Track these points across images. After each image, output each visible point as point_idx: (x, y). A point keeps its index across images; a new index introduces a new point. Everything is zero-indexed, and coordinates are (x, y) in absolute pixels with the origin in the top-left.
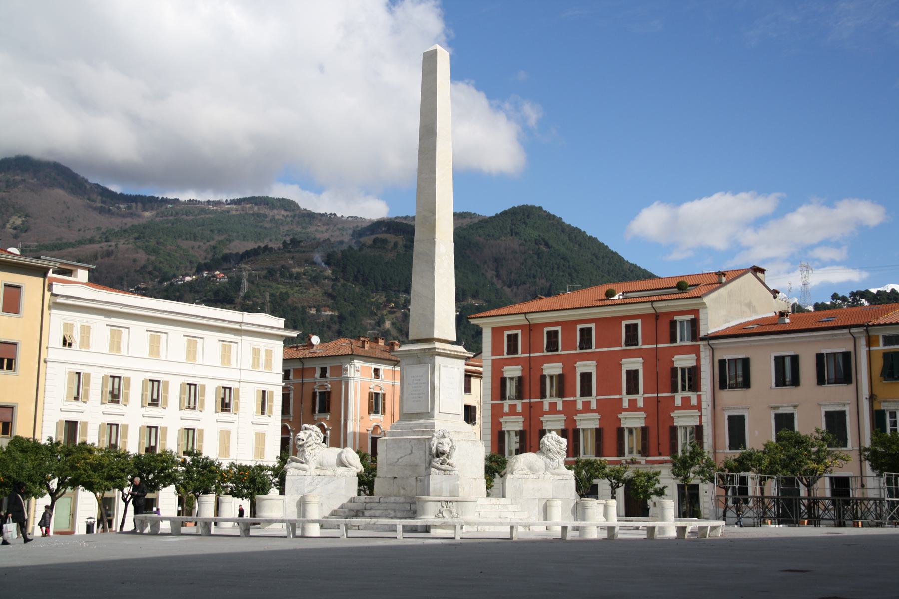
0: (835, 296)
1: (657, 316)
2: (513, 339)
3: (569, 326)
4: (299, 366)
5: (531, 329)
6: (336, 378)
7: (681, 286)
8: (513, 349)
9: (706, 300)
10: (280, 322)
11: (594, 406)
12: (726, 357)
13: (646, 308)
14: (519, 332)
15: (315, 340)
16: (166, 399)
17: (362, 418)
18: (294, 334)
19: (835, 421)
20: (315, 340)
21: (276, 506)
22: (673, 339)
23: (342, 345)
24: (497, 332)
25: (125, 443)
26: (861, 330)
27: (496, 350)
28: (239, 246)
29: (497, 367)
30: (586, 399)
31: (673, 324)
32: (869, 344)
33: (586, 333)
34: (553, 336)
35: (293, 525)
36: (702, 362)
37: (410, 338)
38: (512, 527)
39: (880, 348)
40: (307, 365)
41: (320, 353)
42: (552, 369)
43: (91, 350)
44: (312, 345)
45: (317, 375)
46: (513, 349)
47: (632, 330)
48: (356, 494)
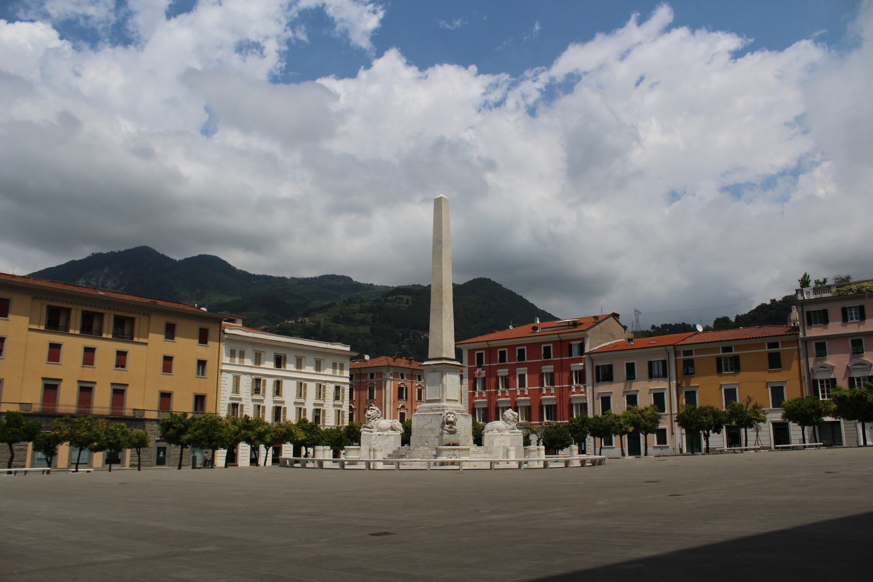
0: (653, 327)
1: (561, 342)
2: (480, 356)
3: (512, 348)
4: (358, 372)
5: (491, 350)
6: (379, 379)
7: (575, 324)
8: (480, 361)
9: (588, 332)
10: (348, 349)
11: (526, 393)
12: (600, 364)
13: (555, 338)
14: (483, 352)
15: (367, 357)
18: (356, 354)
19: (659, 398)
20: (367, 357)
21: (350, 453)
22: (570, 355)
23: (383, 361)
24: (471, 352)
25: (263, 416)
26: (671, 347)
27: (471, 362)
28: (316, 303)
30: (522, 389)
31: (570, 346)
32: (676, 356)
33: (521, 352)
34: (503, 354)
35: (368, 463)
37: (429, 357)
38: (491, 463)
39: (682, 357)
40: (363, 372)
41: (369, 365)
42: (503, 372)
43: (303, 370)
44: (365, 361)
45: (369, 377)
46: (480, 361)
47: (547, 350)
48: (400, 445)
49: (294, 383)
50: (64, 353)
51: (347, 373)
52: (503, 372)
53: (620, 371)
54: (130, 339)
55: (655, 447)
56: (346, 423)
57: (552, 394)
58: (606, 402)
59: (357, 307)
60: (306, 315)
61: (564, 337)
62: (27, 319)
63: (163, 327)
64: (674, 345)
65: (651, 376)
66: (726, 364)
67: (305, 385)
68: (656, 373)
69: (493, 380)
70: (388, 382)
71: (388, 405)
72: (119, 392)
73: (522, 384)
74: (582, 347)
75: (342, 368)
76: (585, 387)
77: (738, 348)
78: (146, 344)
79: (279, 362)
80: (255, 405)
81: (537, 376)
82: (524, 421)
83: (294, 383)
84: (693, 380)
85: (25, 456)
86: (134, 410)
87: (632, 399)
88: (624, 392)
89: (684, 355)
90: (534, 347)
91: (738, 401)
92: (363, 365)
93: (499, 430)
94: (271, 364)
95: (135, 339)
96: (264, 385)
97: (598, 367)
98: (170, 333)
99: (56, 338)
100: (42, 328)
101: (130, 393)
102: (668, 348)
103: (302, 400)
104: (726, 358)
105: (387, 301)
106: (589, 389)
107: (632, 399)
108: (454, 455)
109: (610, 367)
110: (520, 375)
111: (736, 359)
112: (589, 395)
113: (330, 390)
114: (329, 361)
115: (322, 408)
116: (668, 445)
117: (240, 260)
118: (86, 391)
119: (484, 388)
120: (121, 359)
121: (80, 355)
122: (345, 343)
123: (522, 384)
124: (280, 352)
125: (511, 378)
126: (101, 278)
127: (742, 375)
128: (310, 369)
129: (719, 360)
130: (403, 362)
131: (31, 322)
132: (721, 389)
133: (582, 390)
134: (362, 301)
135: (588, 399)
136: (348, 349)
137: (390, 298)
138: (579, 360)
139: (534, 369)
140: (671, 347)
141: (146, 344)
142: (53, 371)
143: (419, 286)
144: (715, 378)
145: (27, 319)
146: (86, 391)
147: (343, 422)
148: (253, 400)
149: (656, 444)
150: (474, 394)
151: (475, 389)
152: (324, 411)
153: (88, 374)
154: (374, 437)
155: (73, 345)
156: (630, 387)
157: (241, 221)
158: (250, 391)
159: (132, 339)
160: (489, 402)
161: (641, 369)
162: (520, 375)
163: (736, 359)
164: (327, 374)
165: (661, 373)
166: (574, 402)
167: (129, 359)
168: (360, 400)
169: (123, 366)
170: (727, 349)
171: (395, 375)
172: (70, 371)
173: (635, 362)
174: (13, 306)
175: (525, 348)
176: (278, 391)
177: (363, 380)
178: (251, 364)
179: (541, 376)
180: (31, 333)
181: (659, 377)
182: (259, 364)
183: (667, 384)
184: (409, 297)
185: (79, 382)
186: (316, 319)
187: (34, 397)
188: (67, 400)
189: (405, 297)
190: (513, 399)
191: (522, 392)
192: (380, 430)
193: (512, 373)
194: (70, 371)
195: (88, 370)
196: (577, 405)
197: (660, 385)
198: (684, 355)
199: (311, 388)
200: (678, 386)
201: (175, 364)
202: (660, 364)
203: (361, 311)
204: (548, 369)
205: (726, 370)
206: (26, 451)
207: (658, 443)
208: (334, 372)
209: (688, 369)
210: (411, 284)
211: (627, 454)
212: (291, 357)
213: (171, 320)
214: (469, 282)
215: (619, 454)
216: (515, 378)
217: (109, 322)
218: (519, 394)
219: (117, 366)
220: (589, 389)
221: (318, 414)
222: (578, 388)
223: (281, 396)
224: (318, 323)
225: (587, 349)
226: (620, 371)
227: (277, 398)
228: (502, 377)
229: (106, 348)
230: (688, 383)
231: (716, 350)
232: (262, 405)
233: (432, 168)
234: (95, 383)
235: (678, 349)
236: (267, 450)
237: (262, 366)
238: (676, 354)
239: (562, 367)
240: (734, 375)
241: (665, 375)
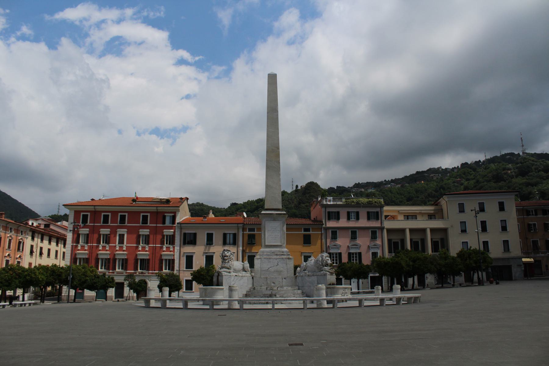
3: (114, 213)
11: (125, 249)
22: (164, 223)
30: (121, 245)
31: (164, 217)
32: (243, 231)
36: (176, 233)
39: (247, 232)
52: (105, 231)
53: (202, 238)
73: (121, 242)
74: (174, 218)
76: (174, 247)
84: (254, 248)
97: (185, 234)
106: (177, 248)
110: (120, 235)
123: (121, 242)
132: (301, 256)
133: (172, 249)
135: (175, 256)
138: (171, 228)
149: (184, 290)
160: (91, 253)
161: (218, 238)
162: (120, 235)
165: (232, 241)
175: (89, 214)
200: (244, 251)
204: (145, 232)
216: (115, 236)
218: (118, 249)
220: (177, 248)
226: (202, 238)
238: (244, 230)
241: (235, 243)
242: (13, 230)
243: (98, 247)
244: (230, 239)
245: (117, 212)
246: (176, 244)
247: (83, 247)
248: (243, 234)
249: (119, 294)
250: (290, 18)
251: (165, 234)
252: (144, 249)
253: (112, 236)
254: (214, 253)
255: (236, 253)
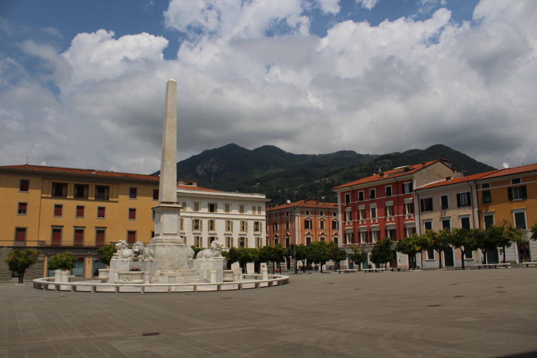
2: (348, 196)
3: (366, 189)
4: (280, 212)
5: (354, 192)
8: (348, 201)
10: (264, 197)
11: (377, 222)
12: (423, 198)
13: (392, 180)
14: (349, 193)
16: (261, 228)
17: (302, 230)
22: (404, 192)
24: (342, 194)
26: (472, 182)
29: (343, 208)
30: (374, 218)
31: (403, 186)
32: (477, 189)
33: (373, 192)
34: (361, 194)
36: (415, 201)
39: (481, 189)
42: (362, 207)
43: (230, 213)
44: (288, 204)
46: (348, 201)
49: (224, 221)
50: (64, 210)
51: (264, 213)
52: (362, 207)
53: (437, 203)
54: (106, 199)
55: (427, 261)
56: (264, 244)
57: (393, 222)
58: (428, 225)
59: (357, 169)
60: (327, 176)
61: (399, 179)
62: (40, 191)
63: (128, 191)
64: (474, 180)
65: (459, 205)
66: (516, 193)
67: (232, 222)
68: (464, 203)
69: (356, 213)
70: (297, 218)
71: (297, 233)
72: (100, 233)
73: (374, 216)
74: (411, 185)
75: (260, 209)
76: (414, 216)
77: (525, 179)
78: (117, 202)
79: (212, 208)
80: (195, 237)
81: (383, 209)
82: (350, 243)
83: (224, 221)
84: (490, 207)
85: (43, 272)
86: (111, 242)
87: (446, 224)
88: (441, 218)
89: (483, 188)
90: (380, 187)
91: (494, 224)
92: (287, 206)
93: (207, 257)
94: (206, 210)
95: (110, 199)
96: (201, 223)
97: (422, 200)
98: (133, 194)
99: (59, 202)
100: (50, 196)
101: (108, 233)
102: (470, 183)
103: (230, 232)
104: (515, 188)
105: (376, 164)
106: (417, 217)
107: (446, 224)
108: (127, 278)
109: (430, 200)
110: (372, 209)
111: (524, 188)
112: (416, 221)
113: (251, 225)
114: (250, 206)
115: (245, 237)
116: (473, 258)
117: (285, 146)
118: (79, 232)
119: (351, 219)
120: (101, 212)
121: (74, 211)
122: (260, 192)
123: (374, 216)
124: (212, 202)
125: (367, 211)
126: (210, 164)
127: (529, 202)
128: (236, 212)
129: (510, 190)
130: (312, 204)
131: (42, 193)
132: (512, 213)
133: (412, 218)
134: (361, 165)
135: (416, 224)
136: (264, 197)
137: (378, 162)
138: (410, 196)
139: (381, 204)
140: (472, 182)
141: (117, 202)
142: (58, 221)
143: (398, 153)
144: (508, 204)
145: (40, 191)
146: (79, 232)
147: (261, 245)
148: (194, 234)
149: (427, 259)
150: (345, 223)
151: (345, 220)
152: (247, 239)
153: (80, 222)
154: (118, 263)
155: (70, 205)
156: (445, 215)
157: (280, 125)
158: (191, 228)
159: (88, 198)
160: (354, 228)
161: (452, 201)
162: (372, 209)
163: (524, 188)
164: (249, 214)
165: (467, 203)
166: (407, 227)
167: (107, 212)
168: (281, 231)
169: (103, 216)
170: (518, 181)
171: (302, 213)
172: (69, 221)
173: (448, 195)
174: (31, 184)
175: (375, 189)
176: (212, 226)
177: (282, 217)
178: (191, 211)
179: (386, 208)
180: (43, 199)
181: (465, 205)
182: (198, 210)
183: (471, 211)
184: (391, 161)
185: (75, 227)
186: (332, 179)
187: (47, 237)
188: (68, 238)
189: (387, 161)
190: (368, 226)
191: (374, 220)
192: (124, 257)
193: (367, 208)
194: (69, 221)
195: (80, 219)
196: (409, 229)
197: (466, 212)
198: (483, 188)
199: (237, 225)
200: (479, 212)
201: (137, 213)
202: (466, 195)
203: (360, 172)
204: (390, 203)
205: (516, 198)
206: (43, 269)
207: (429, 258)
208: (254, 213)
209: (487, 198)
210: (393, 152)
211: (444, 266)
212: (220, 204)
213: (133, 186)
214: (429, 148)
215: (438, 266)
216: (369, 211)
217: (92, 190)
218: (372, 222)
219: (99, 216)
220: (417, 217)
221: (242, 241)
222: (409, 217)
223: (214, 230)
224: (334, 181)
225: (415, 187)
226: (437, 203)
227: (211, 232)
228: (362, 211)
229: (91, 206)
230: (486, 210)
231: (507, 182)
232: (200, 236)
233: (385, 76)
234: (85, 227)
235: (478, 183)
236: (440, 252)
237: (200, 211)
238: (477, 187)
239: (399, 202)
240: (522, 201)
241: (469, 204)
242: (323, 213)
243: (404, 217)
244: (463, 200)
245: (383, 186)
246: (415, 212)
247: (390, 219)
248: (477, 192)
249: (524, 253)
250: (112, 33)
251: (387, 205)
252: (391, 221)
253: (367, 211)
254: (450, 217)
255: (472, 215)
